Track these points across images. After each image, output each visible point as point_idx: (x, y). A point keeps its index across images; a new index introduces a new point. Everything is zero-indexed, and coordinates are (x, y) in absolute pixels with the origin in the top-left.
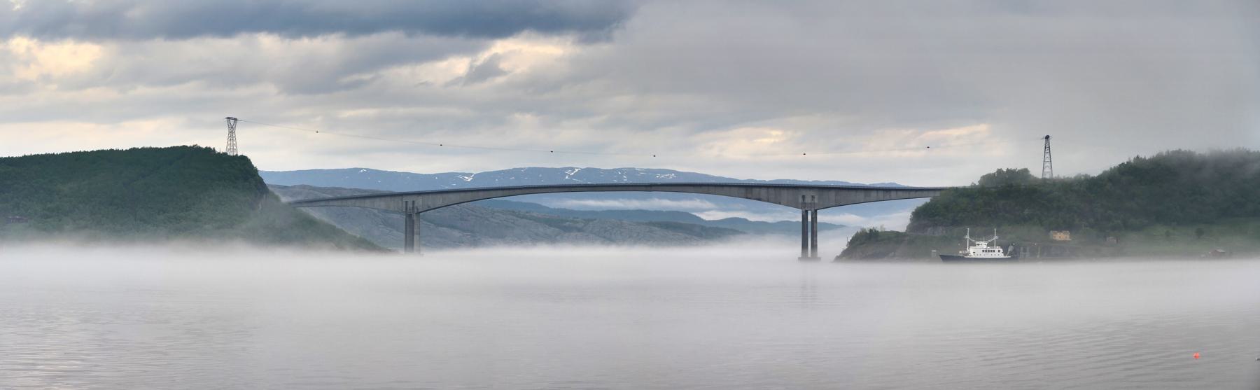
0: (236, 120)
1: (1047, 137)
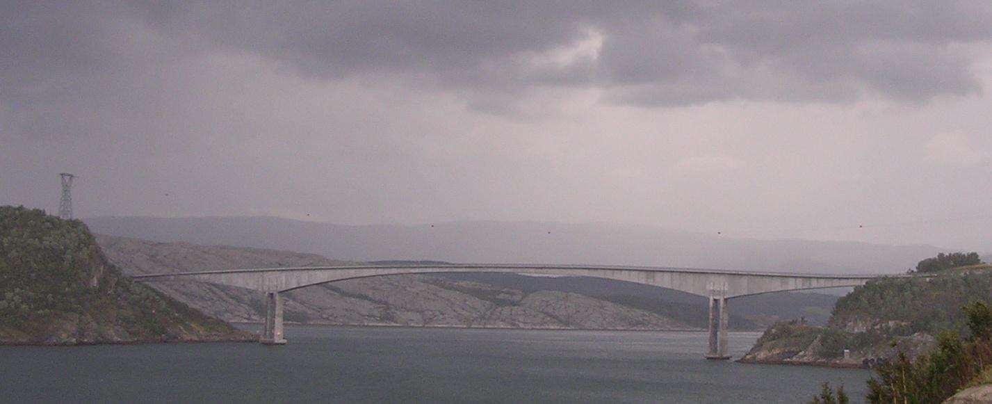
0: (72, 176)
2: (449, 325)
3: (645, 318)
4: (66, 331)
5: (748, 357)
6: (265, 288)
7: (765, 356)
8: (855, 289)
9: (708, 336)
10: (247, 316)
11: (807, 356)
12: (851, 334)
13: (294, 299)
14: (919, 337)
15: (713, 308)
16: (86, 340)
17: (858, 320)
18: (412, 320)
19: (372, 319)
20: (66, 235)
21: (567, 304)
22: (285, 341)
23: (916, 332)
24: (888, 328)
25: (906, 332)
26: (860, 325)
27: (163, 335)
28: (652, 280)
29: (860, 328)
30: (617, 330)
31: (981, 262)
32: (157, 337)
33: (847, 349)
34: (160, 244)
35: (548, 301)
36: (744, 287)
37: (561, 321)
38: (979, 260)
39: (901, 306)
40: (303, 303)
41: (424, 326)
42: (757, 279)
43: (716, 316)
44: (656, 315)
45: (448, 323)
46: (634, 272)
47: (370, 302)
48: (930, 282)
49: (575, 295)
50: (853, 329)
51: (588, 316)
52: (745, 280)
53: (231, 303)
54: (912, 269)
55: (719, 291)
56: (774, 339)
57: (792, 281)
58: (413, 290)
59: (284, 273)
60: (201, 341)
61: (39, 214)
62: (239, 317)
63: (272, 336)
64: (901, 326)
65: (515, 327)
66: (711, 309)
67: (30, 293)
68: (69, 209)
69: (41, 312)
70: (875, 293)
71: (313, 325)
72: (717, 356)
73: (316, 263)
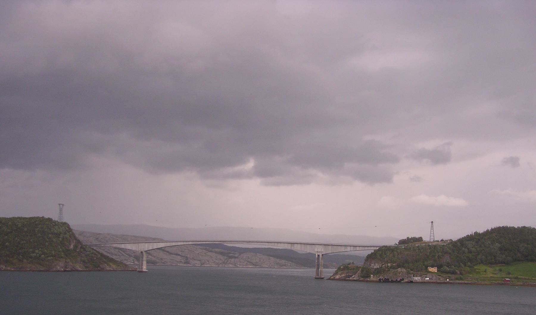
0: (63, 205)
1: (432, 222)
2: (211, 266)
3: (286, 263)
4: (60, 265)
5: (332, 277)
6: (139, 250)
7: (339, 277)
8: (374, 251)
9: (315, 270)
10: (133, 262)
11: (355, 277)
12: (373, 269)
13: (151, 255)
14: (401, 270)
15: (317, 258)
16: (67, 270)
17: (376, 263)
18: (196, 264)
19: (181, 263)
20: (61, 228)
21: (256, 258)
22: (147, 271)
23: (399, 268)
24: (388, 266)
25: (395, 268)
26: (377, 265)
27: (99, 268)
28: (293, 247)
29: (377, 266)
30: (275, 268)
31: (424, 240)
32: (96, 269)
33: (372, 274)
34: (99, 234)
35: (248, 257)
36: (330, 250)
37: (254, 265)
38: (423, 240)
39: (393, 257)
40: (154, 257)
41: (201, 266)
42: (335, 247)
43: (318, 262)
44: (290, 262)
45: (210, 265)
46: (286, 244)
47: (180, 257)
48: (404, 248)
49: (259, 254)
50: (374, 267)
51: (264, 262)
52: (330, 247)
53: (127, 257)
54: (396, 243)
55: (320, 252)
56: (342, 270)
57: (349, 248)
58: (197, 252)
59: (147, 244)
60: (114, 270)
61: (50, 220)
62: (130, 262)
63: (142, 268)
64: (393, 266)
65: (236, 267)
66: (316, 259)
67: (45, 251)
68: (62, 218)
69: (49, 258)
70: (382, 252)
71: (158, 265)
72: (319, 277)
73: (161, 241)
